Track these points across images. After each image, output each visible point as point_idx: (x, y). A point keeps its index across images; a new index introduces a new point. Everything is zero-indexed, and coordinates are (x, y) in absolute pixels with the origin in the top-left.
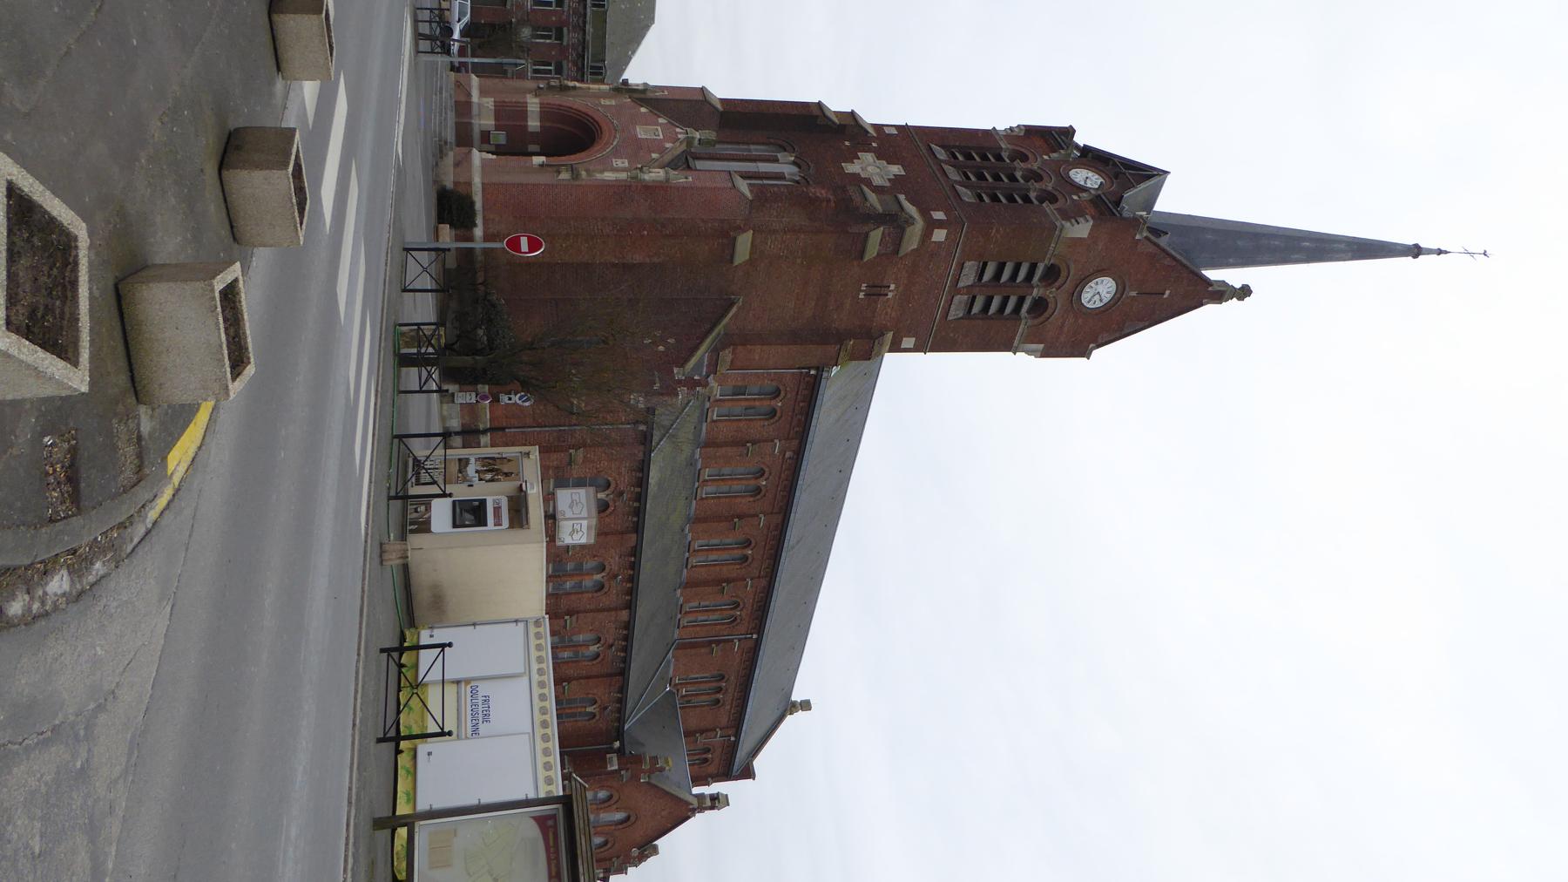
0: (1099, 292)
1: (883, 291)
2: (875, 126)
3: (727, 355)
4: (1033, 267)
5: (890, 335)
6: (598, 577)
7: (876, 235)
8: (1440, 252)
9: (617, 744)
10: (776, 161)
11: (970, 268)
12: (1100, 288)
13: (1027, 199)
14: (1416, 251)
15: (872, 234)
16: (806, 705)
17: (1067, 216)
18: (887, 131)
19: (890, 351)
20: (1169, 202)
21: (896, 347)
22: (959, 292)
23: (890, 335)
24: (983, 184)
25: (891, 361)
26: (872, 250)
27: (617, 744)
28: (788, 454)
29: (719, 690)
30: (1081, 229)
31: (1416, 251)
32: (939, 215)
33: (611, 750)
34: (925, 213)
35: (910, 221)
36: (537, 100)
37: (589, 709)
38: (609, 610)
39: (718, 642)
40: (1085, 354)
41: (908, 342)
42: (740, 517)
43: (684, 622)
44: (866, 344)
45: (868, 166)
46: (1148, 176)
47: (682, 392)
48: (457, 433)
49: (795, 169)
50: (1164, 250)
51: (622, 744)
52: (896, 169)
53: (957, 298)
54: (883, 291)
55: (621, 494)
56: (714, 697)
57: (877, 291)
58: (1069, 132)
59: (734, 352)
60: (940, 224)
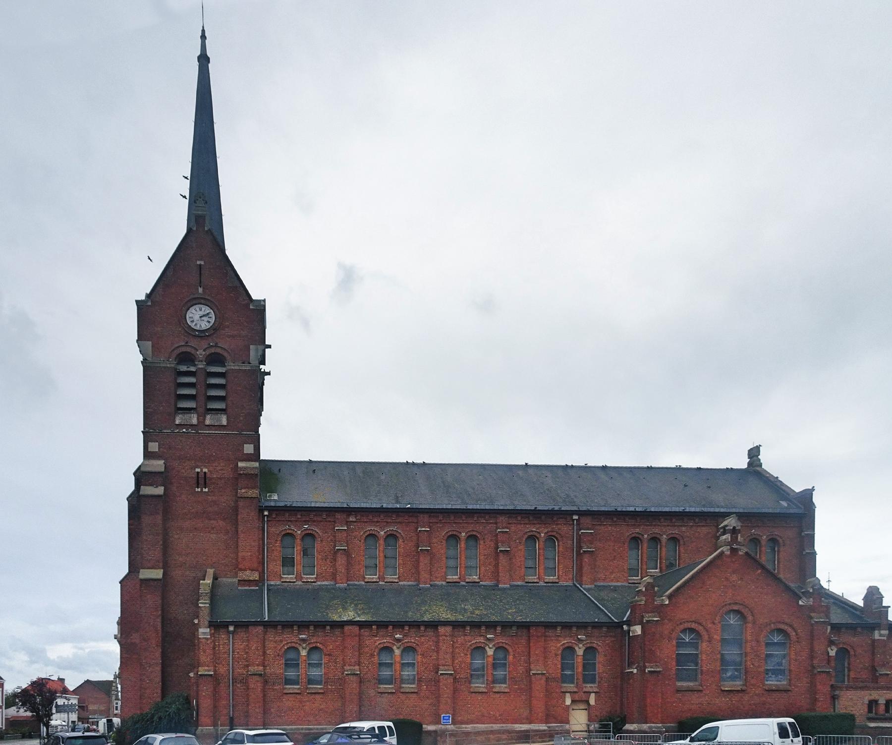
1: (201, 475)
8: (203, 37)
14: (204, 60)
16: (754, 453)
31: (204, 60)
54: (201, 475)
55: (489, 639)
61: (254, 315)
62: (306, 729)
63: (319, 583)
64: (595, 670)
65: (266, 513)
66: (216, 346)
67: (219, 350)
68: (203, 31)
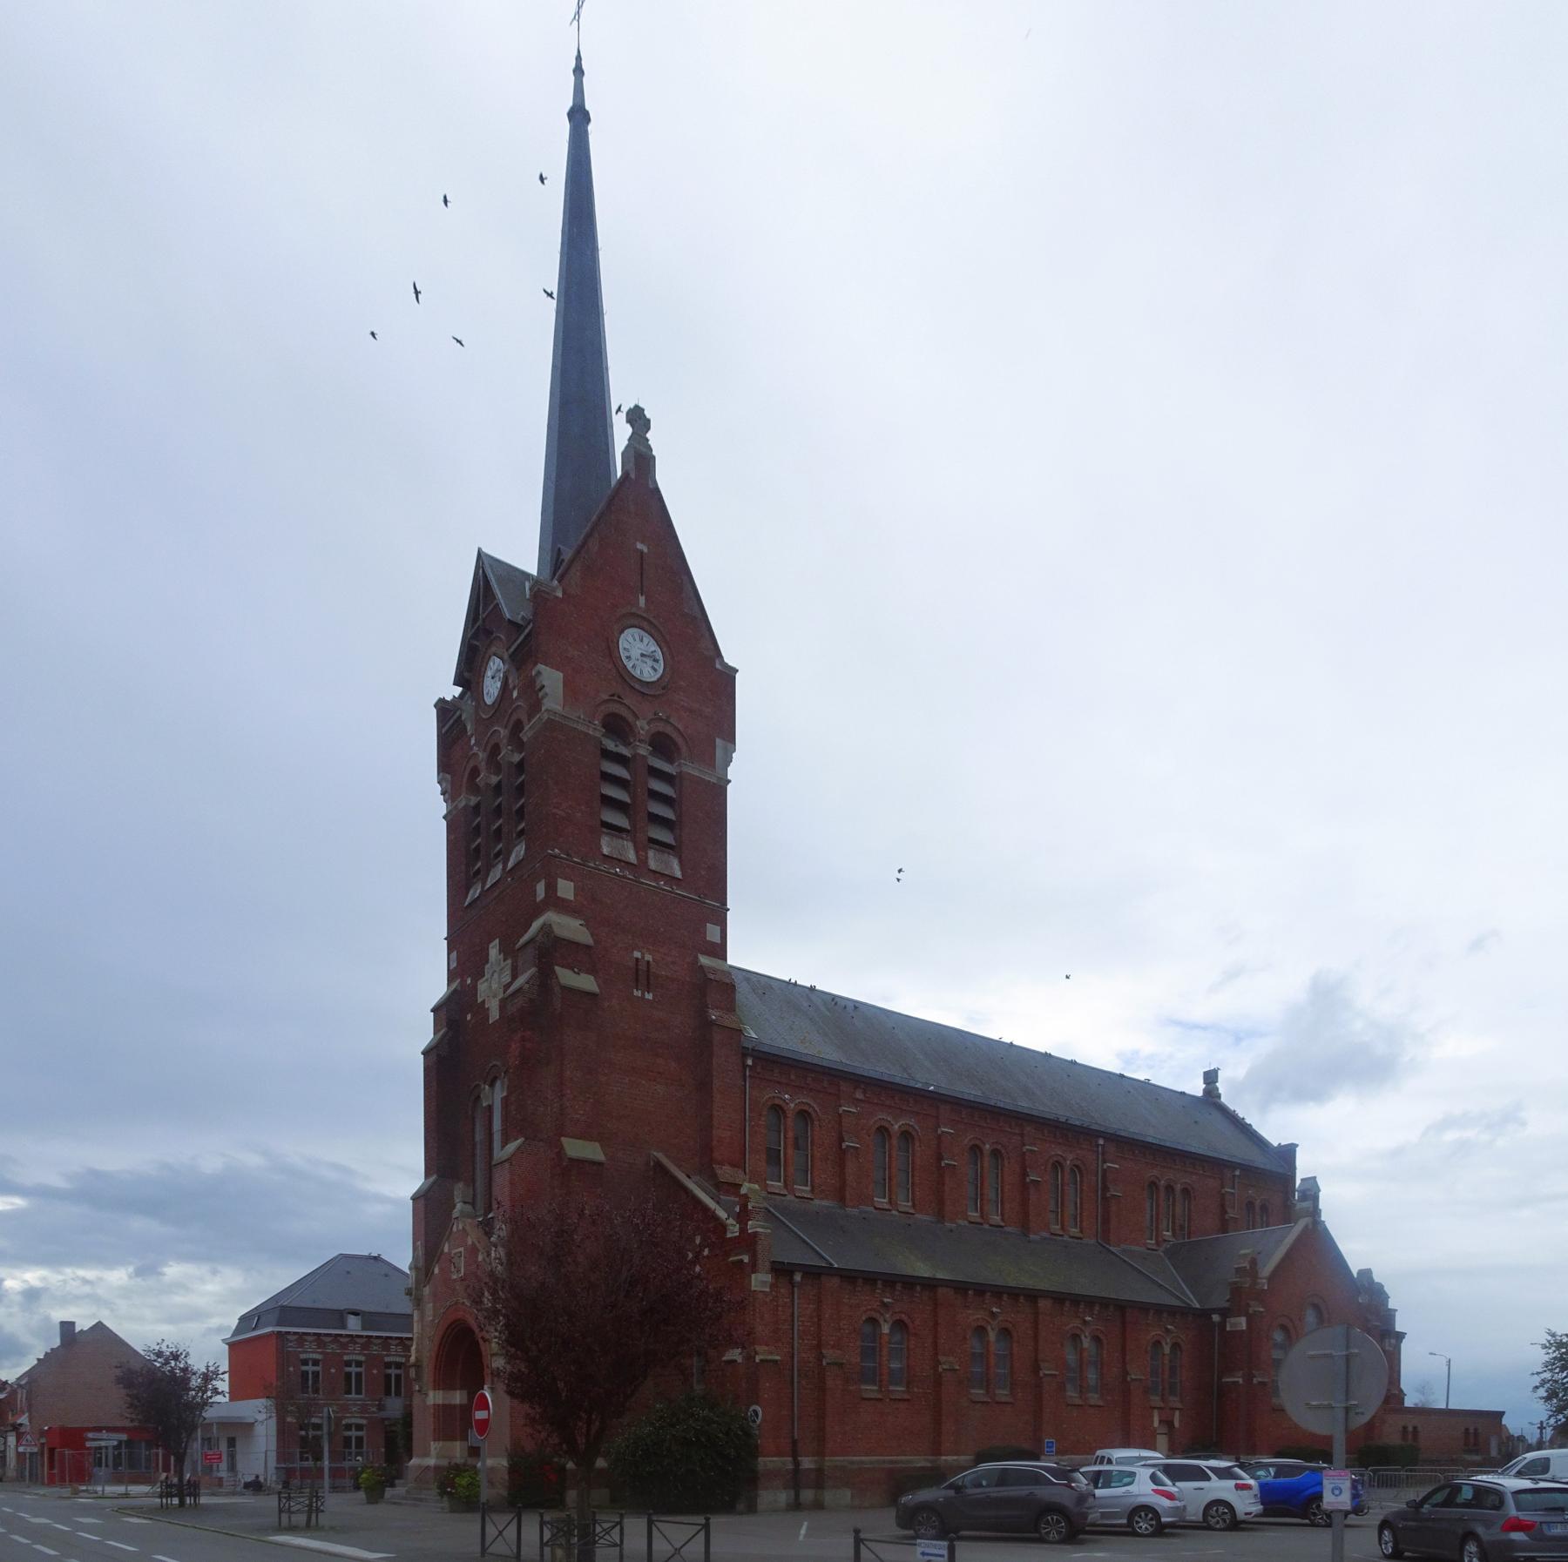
0: (639, 652)
1: (643, 967)
2: (450, 981)
3: (726, 1173)
4: (607, 755)
5: (704, 960)
6: (992, 1336)
7: (566, 977)
8: (579, 71)
9: (1216, 1318)
10: (490, 1108)
11: (607, 846)
12: (635, 653)
13: (520, 767)
14: (579, 116)
15: (563, 981)
16: (1211, 1077)
17: (535, 706)
18: (454, 965)
19: (725, 959)
20: (523, 551)
21: (720, 950)
22: (643, 862)
23: (704, 960)
24: (505, 830)
25: (737, 957)
26: (587, 982)
27: (1216, 1318)
28: (859, 1095)
29: (1170, 1188)
30: (551, 679)
31: (579, 116)
32: (541, 889)
33: (1223, 1324)
34: (538, 910)
35: (547, 929)
36: (431, 1393)
37: (1167, 1350)
38: (1036, 1323)
39: (1105, 1188)
40: (729, 675)
41: (712, 932)
42: (940, 1158)
43: (1074, 1231)
44: (718, 988)
45: (491, 990)
46: (489, 580)
47: (752, 1226)
48: (797, 1496)
49: (498, 1084)
50: (578, 552)
51: (1214, 1311)
52: (494, 951)
53: (653, 865)
54: (643, 967)
55: (885, 1305)
56: (1162, 1194)
57: (643, 976)
58: (443, 708)
59: (721, 1163)
60: (551, 888)
61: (717, 685)
62: (892, 1462)
63: (817, 1202)
64: (411, 1331)
65: (750, 1062)
66: (667, 721)
67: (669, 730)
68: (579, 58)
